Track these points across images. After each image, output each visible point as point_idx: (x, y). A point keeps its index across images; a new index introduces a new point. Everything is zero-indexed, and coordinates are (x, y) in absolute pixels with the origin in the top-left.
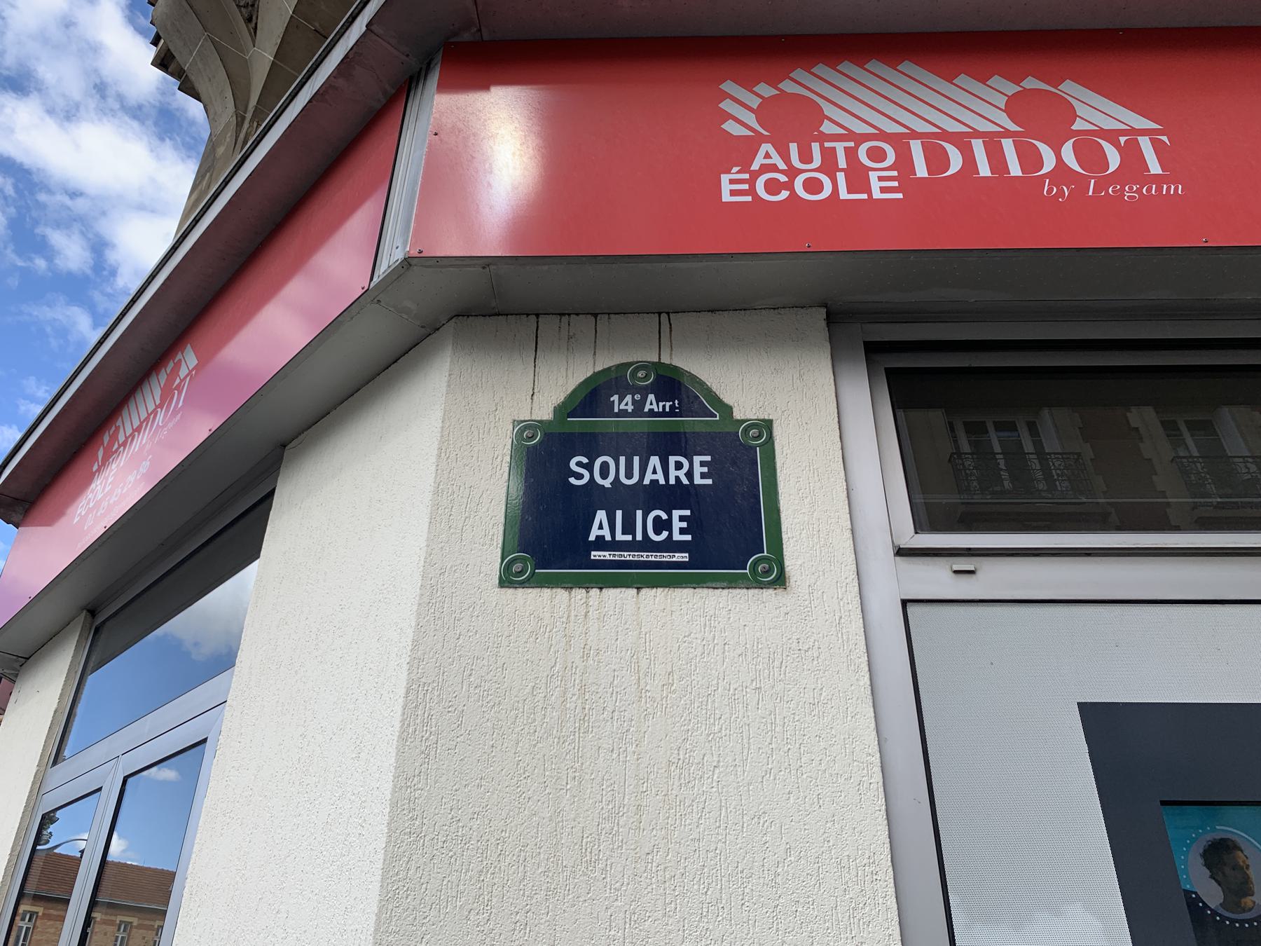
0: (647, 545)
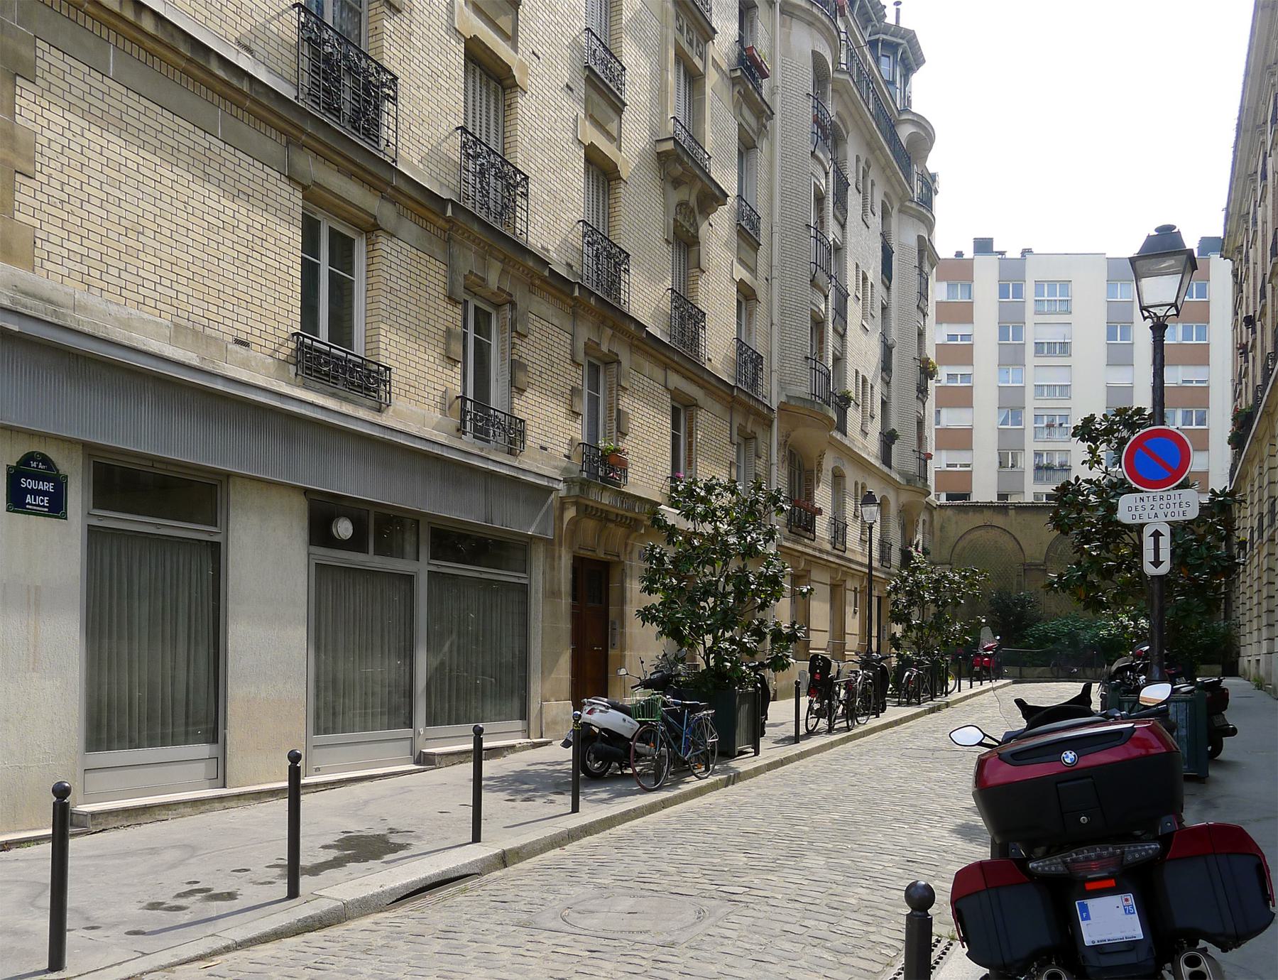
0: (39, 505)
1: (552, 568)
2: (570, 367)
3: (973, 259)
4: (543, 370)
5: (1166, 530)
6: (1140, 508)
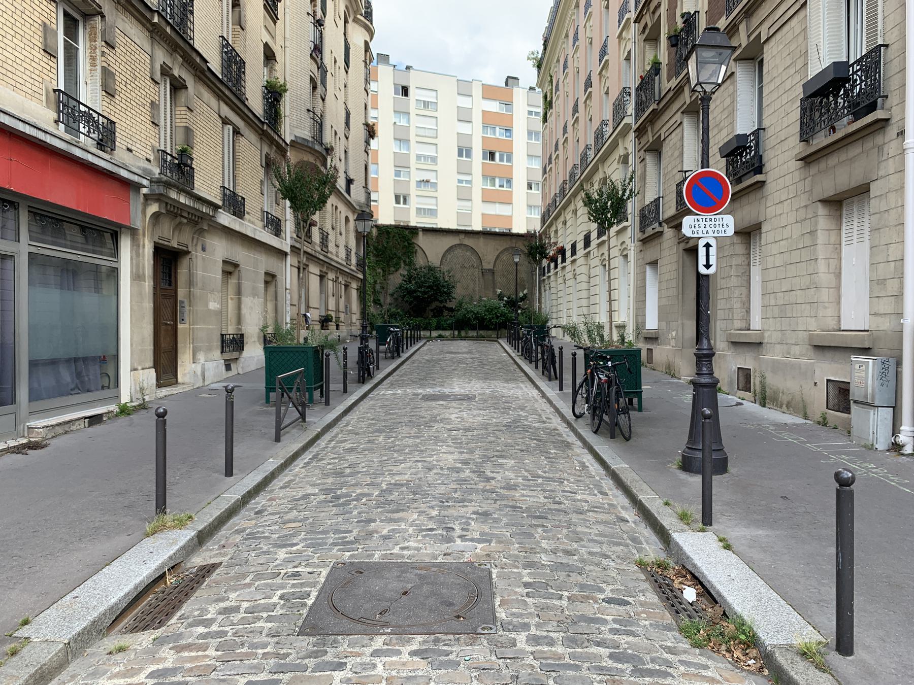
1: (138, 255)
2: (149, 84)
3: (388, 63)
4: (128, 82)
5: (713, 242)
6: (697, 226)
